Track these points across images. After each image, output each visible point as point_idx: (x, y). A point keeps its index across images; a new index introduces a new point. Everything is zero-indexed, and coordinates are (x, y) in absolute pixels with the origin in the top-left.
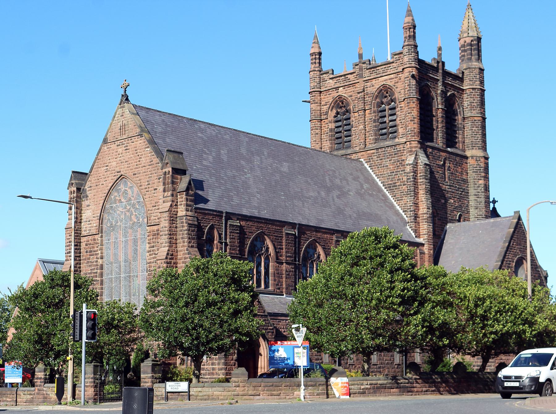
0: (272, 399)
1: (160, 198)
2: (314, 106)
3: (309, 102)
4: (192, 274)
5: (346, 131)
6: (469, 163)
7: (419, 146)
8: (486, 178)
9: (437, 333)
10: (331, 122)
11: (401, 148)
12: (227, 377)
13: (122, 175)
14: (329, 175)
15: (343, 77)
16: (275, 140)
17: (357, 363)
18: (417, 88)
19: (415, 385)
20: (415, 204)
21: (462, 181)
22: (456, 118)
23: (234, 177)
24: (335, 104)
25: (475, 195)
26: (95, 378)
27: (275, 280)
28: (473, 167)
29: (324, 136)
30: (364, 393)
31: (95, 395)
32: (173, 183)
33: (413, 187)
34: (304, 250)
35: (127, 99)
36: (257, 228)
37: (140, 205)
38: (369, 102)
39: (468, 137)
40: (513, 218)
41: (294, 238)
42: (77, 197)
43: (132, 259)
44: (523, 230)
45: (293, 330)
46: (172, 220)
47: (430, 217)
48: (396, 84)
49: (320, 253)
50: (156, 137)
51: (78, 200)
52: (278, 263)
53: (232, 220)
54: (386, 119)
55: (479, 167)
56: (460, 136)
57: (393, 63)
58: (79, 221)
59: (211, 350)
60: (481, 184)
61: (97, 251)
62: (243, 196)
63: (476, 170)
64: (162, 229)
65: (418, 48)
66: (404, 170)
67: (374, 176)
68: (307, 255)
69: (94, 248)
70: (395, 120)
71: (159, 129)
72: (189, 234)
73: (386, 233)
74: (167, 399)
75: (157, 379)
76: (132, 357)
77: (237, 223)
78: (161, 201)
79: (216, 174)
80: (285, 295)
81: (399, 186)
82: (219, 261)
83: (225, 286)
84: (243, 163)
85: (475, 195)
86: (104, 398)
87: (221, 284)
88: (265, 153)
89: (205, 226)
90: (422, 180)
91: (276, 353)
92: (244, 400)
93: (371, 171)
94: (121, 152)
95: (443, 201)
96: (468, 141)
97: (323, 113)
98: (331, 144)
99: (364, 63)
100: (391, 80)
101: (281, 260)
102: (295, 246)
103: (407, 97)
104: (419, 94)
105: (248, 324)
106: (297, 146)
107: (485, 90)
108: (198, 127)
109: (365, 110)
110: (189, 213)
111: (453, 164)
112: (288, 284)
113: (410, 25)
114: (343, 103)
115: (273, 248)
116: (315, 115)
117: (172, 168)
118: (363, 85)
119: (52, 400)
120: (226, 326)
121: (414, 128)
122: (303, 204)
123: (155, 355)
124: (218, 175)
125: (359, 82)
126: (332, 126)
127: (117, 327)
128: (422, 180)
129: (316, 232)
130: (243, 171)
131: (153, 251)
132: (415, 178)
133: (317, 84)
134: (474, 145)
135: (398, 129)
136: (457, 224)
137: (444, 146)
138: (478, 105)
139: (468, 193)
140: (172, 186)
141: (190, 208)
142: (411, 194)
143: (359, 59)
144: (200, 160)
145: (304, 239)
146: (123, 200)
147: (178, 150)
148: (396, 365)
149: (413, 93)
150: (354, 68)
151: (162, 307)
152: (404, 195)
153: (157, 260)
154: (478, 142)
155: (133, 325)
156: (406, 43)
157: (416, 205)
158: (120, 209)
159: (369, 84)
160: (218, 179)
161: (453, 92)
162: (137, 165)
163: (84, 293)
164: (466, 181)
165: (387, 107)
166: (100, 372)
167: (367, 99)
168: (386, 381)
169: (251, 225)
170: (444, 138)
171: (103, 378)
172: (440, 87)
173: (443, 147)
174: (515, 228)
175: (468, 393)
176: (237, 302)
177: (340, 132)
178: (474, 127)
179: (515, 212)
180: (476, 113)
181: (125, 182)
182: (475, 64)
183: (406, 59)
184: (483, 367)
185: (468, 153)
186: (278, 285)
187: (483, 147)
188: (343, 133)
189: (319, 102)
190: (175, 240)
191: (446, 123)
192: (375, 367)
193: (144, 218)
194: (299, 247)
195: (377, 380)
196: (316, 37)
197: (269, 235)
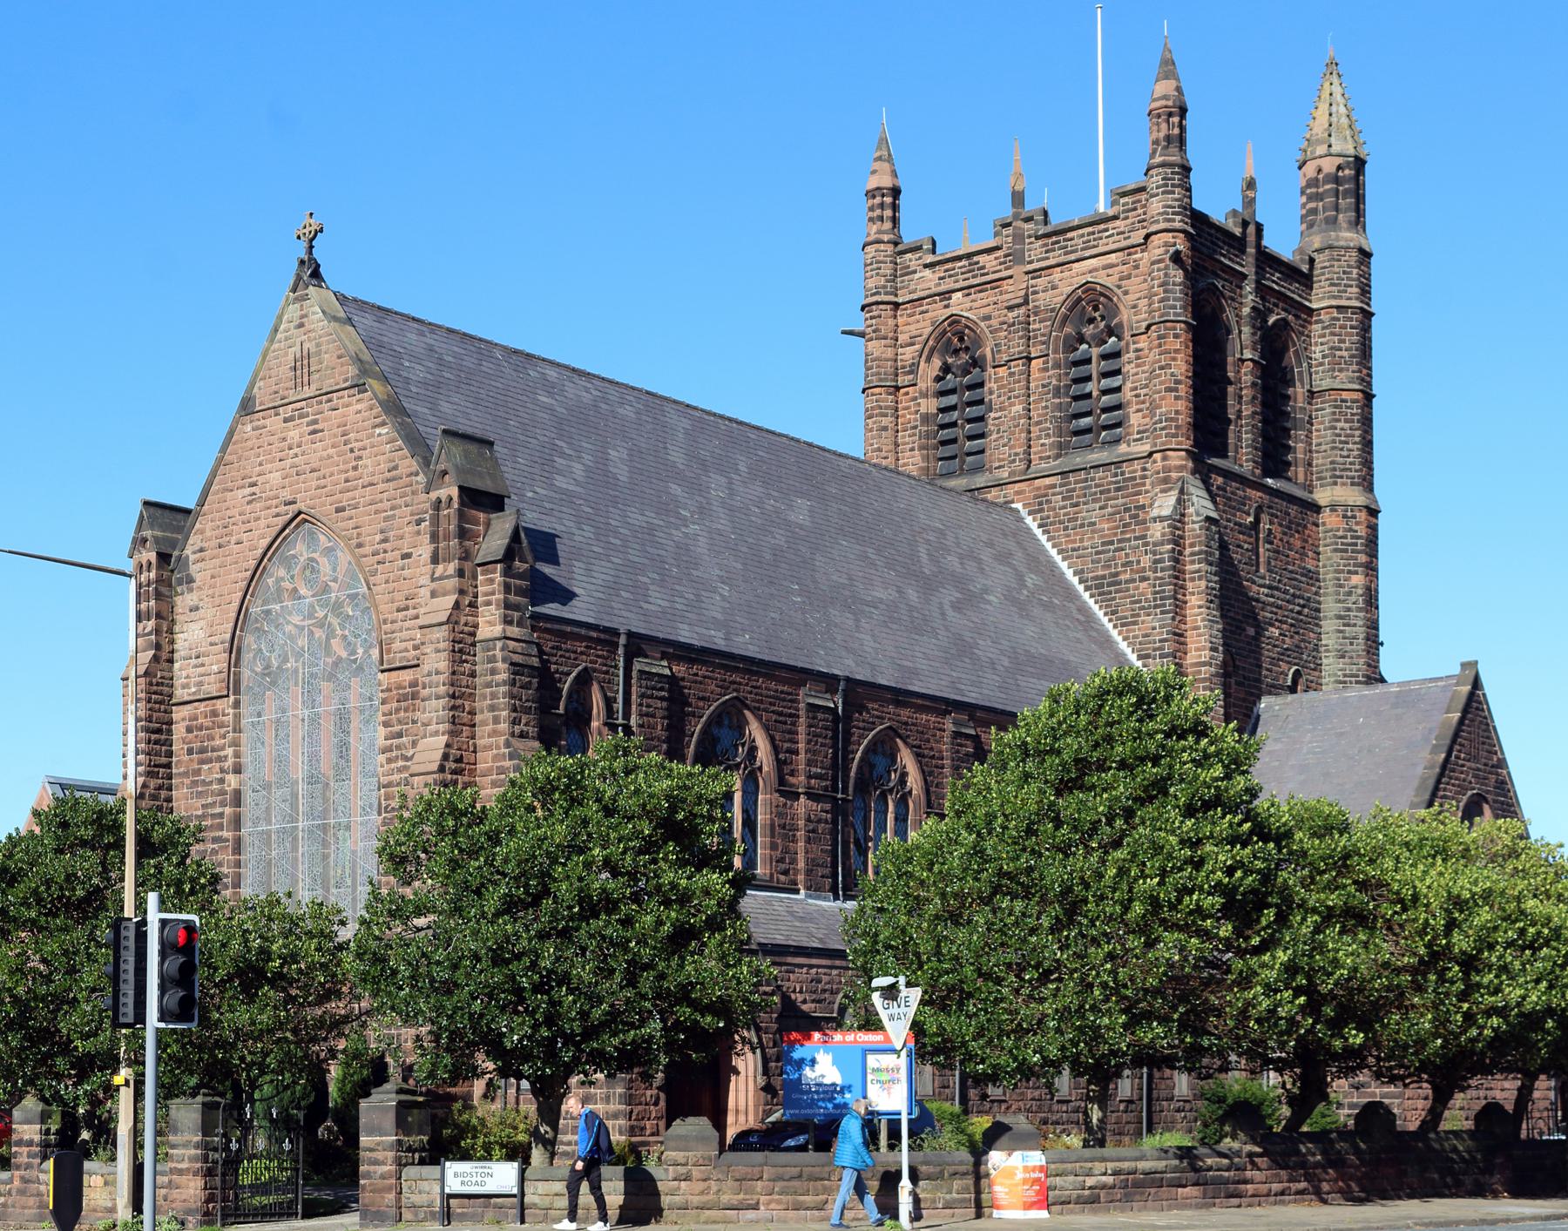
0: (798, 1221)
1: (422, 582)
2: (876, 347)
3: (862, 335)
4: (531, 809)
5: (969, 421)
6: (1324, 524)
7: (1190, 464)
8: (1371, 569)
9: (1328, 1011)
10: (925, 395)
11: (1135, 471)
12: (634, 1139)
13: (300, 513)
14: (928, 542)
15: (964, 263)
16: (768, 431)
17: (1014, 1097)
18: (1186, 294)
19: (1249, 1174)
20: (1175, 634)
21: (1302, 575)
22: (1290, 391)
23: (651, 529)
24: (938, 340)
25: (1339, 617)
26: (206, 1147)
27: (773, 847)
28: (1335, 536)
29: (904, 437)
30: (1093, 1200)
31: (208, 1201)
32: (463, 534)
33: (1170, 584)
34: (862, 759)
35: (316, 274)
36: (721, 687)
37: (357, 605)
38: (1043, 335)
39: (1323, 447)
40: (1459, 680)
41: (833, 721)
42: (159, 580)
43: (332, 773)
44: (1485, 718)
45: (876, 998)
46: (461, 651)
47: (1217, 675)
48: (1123, 283)
49: (907, 770)
50: (408, 394)
51: (164, 590)
52: (782, 793)
53: (646, 656)
54: (1091, 387)
55: (1352, 537)
56: (1300, 445)
57: (1115, 218)
58: (164, 656)
59: (599, 1059)
60: (1356, 587)
61: (223, 748)
62: (678, 587)
63: (1342, 544)
64: (427, 680)
65: (1192, 174)
66: (1144, 537)
67: (1053, 552)
68: (867, 775)
69: (213, 739)
70: (1118, 389)
71: (418, 373)
72: (512, 696)
73: (1167, 686)
74: (447, 1216)
75: (414, 1152)
76: (334, 1071)
77: (662, 668)
78: (425, 592)
79: (597, 518)
80: (802, 891)
81: (1126, 582)
82: (618, 765)
83: (641, 852)
84: (675, 489)
85: (1339, 617)
86: (237, 1208)
87: (631, 840)
88: (742, 468)
89: (562, 673)
90: (1197, 566)
91: (807, 1071)
92: (706, 1223)
93: (1043, 538)
94: (297, 439)
95: (1251, 631)
96: (1320, 461)
97: (903, 367)
98: (926, 458)
99: (1028, 219)
100: (1110, 271)
101: (792, 785)
102: (835, 746)
103: (1157, 320)
104: (1193, 312)
105: (722, 973)
106: (835, 453)
107: (1373, 314)
108: (537, 375)
109: (1029, 359)
110: (514, 631)
111: (1281, 525)
112: (813, 860)
113: (1170, 103)
114: (961, 340)
115: (769, 747)
116: (878, 374)
117: (461, 488)
118: (1024, 285)
120: (646, 981)
121: (1177, 412)
122: (857, 620)
123: (408, 1070)
124: (602, 520)
125: (1011, 277)
126: (930, 405)
127: (279, 980)
128: (1197, 566)
129: (897, 707)
130: (678, 516)
131: (398, 747)
132: (1177, 559)
133: (887, 281)
134: (1338, 473)
135: (1127, 416)
136: (1290, 697)
137: (1258, 472)
138: (1352, 356)
139: (1318, 610)
140: (461, 543)
141: (516, 615)
142: (1164, 605)
143: (1014, 206)
144: (546, 475)
145: (861, 725)
146: (303, 591)
147: (478, 433)
148: (1121, 1101)
149: (1174, 307)
150: (996, 234)
151: (432, 917)
152: (1140, 609)
153: (412, 775)
154: (1351, 463)
155: (334, 975)
156: (1158, 159)
157: (1179, 636)
158: (296, 619)
159: (1041, 282)
160: (603, 532)
161: (1283, 315)
162: (347, 481)
163: (170, 870)
164: (1312, 577)
165: (1095, 352)
166: (224, 1127)
167: (1037, 326)
168: (1164, 1163)
169: (705, 677)
170: (1256, 449)
171: (234, 1146)
172: (1250, 297)
173: (1253, 474)
174: (1466, 711)
175: (1400, 1198)
176: (684, 898)
177: (954, 424)
178: (1339, 421)
179: (1464, 665)
180: (1345, 379)
181: (311, 533)
182: (1347, 236)
183: (1156, 206)
184: (1435, 1115)
185: (1322, 496)
186: (783, 861)
187: (1364, 480)
188: (963, 427)
189: (891, 335)
190: (469, 713)
191: (1264, 404)
192: (1064, 1108)
193: (371, 647)
194: (845, 749)
195: (1137, 1159)
196: (883, 141)
197: (759, 709)
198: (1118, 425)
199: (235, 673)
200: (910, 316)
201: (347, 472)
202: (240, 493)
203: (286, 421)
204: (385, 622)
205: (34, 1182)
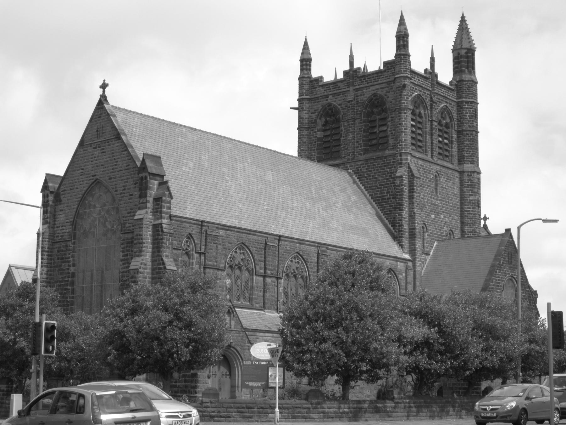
48: (387, 94)
55: (471, 182)
61: (69, 258)
100: (383, 90)
126: (320, 134)
133: (307, 91)
135: (388, 141)
154: (470, 156)
159: (359, 93)
162: (113, 169)
198: (386, 143)
199: (74, 232)
200: (314, 103)
201: (113, 166)
202: (79, 172)
203: (94, 148)
204: (123, 217)
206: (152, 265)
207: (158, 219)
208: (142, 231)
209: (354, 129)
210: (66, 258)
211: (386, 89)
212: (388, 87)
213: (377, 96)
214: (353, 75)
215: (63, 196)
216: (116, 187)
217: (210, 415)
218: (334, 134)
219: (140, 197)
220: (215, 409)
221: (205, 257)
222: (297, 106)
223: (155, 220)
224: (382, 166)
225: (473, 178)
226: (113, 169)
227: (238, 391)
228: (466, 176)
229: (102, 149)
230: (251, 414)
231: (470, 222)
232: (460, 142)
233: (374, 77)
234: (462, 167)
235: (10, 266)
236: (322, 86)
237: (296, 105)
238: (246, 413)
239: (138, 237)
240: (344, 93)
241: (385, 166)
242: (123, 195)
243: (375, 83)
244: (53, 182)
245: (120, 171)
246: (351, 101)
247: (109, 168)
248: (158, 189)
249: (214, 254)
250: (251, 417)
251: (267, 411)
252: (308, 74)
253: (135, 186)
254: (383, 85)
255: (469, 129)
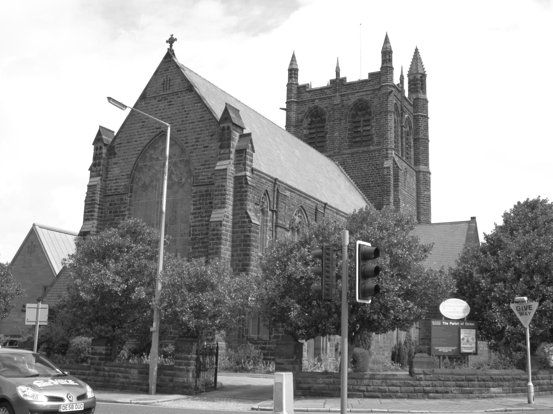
10: (304, 129)
61: (124, 211)
100: (368, 96)
119: (118, 384)
135: (372, 138)
159: (345, 98)
162: (183, 121)
199: (131, 186)
200: (301, 105)
201: (183, 118)
203: (159, 101)
204: (196, 169)
205: (101, 371)
206: (233, 219)
207: (241, 171)
208: (226, 182)
209: (340, 128)
210: (120, 212)
211: (371, 95)
212: (372, 94)
213: (363, 101)
214: (339, 83)
215: (118, 149)
216: (186, 140)
217: (424, 390)
218: (319, 132)
219: (221, 147)
220: (430, 382)
221: (276, 215)
222: (285, 107)
223: (236, 172)
224: (367, 159)
225: (427, 177)
226: (183, 121)
227: (323, 353)
228: (421, 175)
229: (168, 102)
230: (472, 388)
231: (424, 213)
232: (416, 147)
233: (359, 85)
234: (418, 167)
235: (34, 225)
236: (309, 92)
237: (285, 106)
238: (466, 387)
239: (220, 188)
240: (329, 98)
241: (370, 159)
242: (195, 147)
243: (361, 90)
244: (107, 136)
245: (192, 122)
246: (338, 104)
247: (177, 120)
248: (239, 141)
249: (283, 213)
250: (471, 393)
251: (489, 384)
252: (296, 81)
253: (210, 138)
254: (369, 92)
255: (423, 137)
